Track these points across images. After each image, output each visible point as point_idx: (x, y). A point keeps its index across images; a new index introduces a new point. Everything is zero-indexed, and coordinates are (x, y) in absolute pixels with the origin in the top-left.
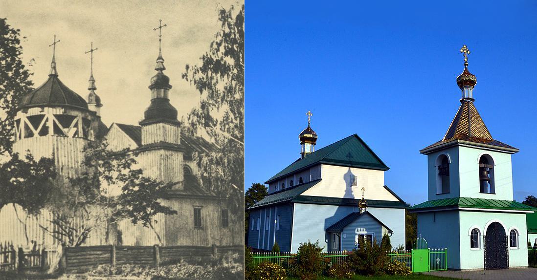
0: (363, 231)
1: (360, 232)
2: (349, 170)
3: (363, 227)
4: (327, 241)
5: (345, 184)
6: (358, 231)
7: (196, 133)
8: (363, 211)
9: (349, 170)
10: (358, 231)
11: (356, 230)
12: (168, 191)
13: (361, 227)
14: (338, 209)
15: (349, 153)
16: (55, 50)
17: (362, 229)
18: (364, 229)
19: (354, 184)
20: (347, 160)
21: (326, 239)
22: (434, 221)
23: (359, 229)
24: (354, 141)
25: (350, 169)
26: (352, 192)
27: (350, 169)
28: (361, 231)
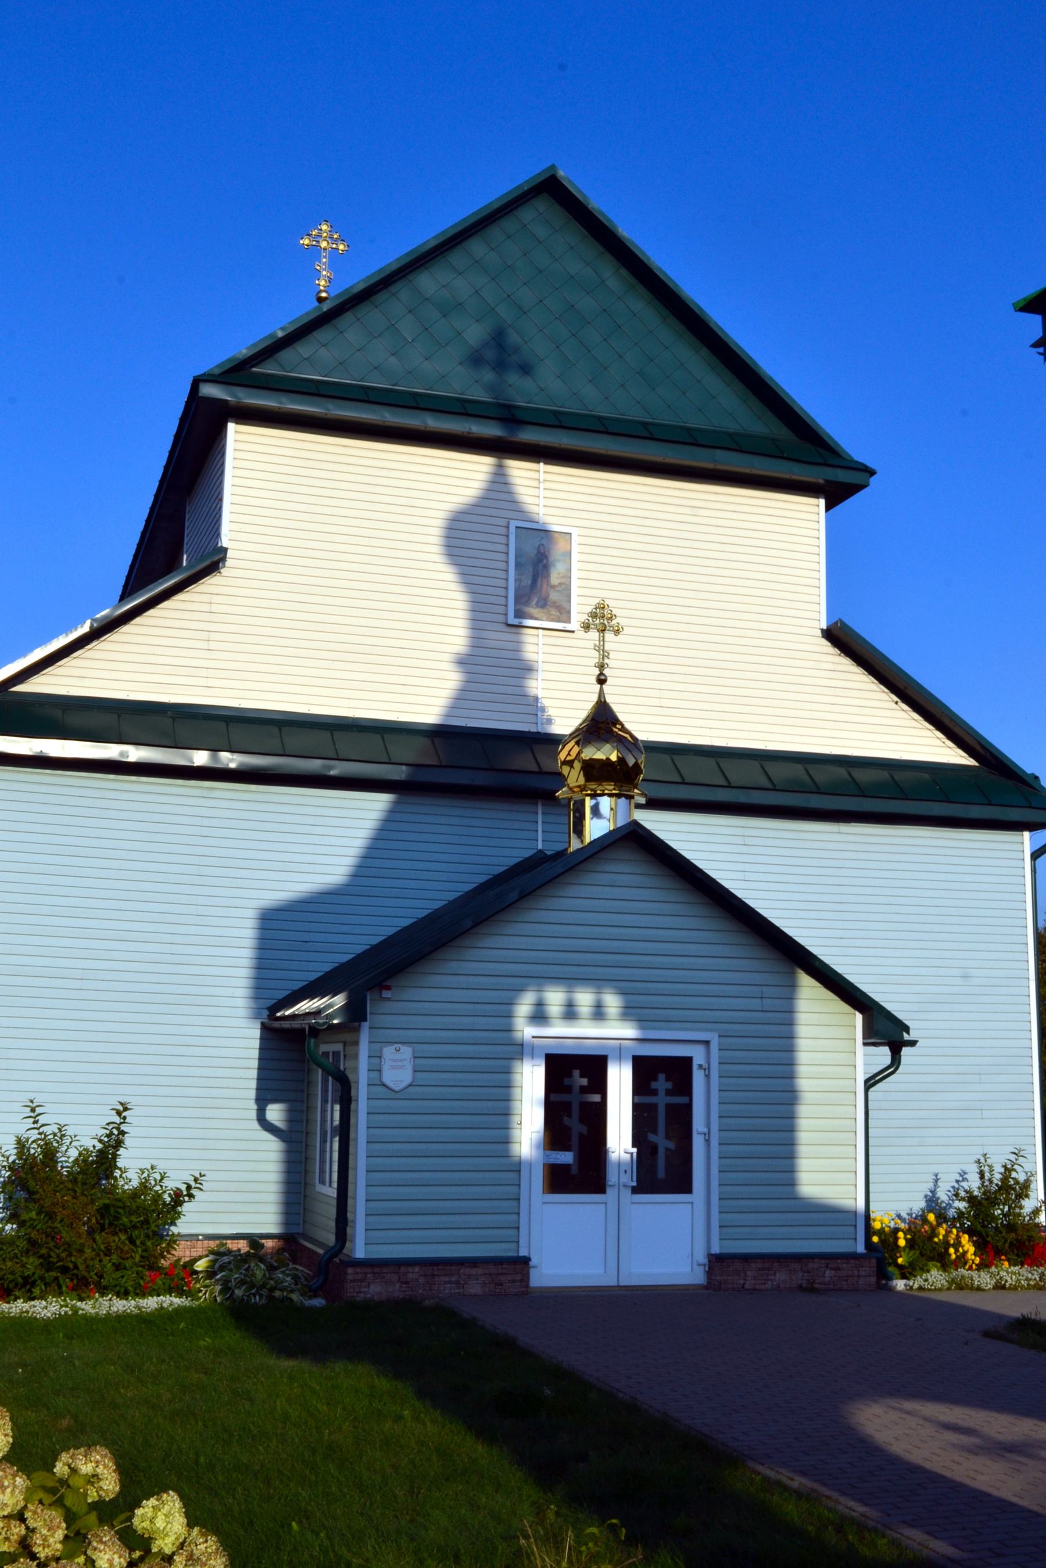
0: (599, 1013)
1: (559, 1029)
2: (499, 482)
3: (597, 982)
4: (275, 1113)
5: (165, 463)
6: (539, 1017)
7: (908, 1033)
8: (595, 829)
9: (499, 482)
10: (539, 1017)
11: (524, 1008)
12: (226, 1506)
13: (570, 980)
14: (396, 803)
15: (498, 338)
16: (495, 603)
17: (584, 999)
18: (612, 1002)
19: (544, 603)
20: (478, 394)
21: (262, 1102)
22: (578, 604)
23: (555, 998)
24: (541, 231)
25: (500, 466)
26: (527, 669)
27: (500, 466)
28: (570, 1013)
